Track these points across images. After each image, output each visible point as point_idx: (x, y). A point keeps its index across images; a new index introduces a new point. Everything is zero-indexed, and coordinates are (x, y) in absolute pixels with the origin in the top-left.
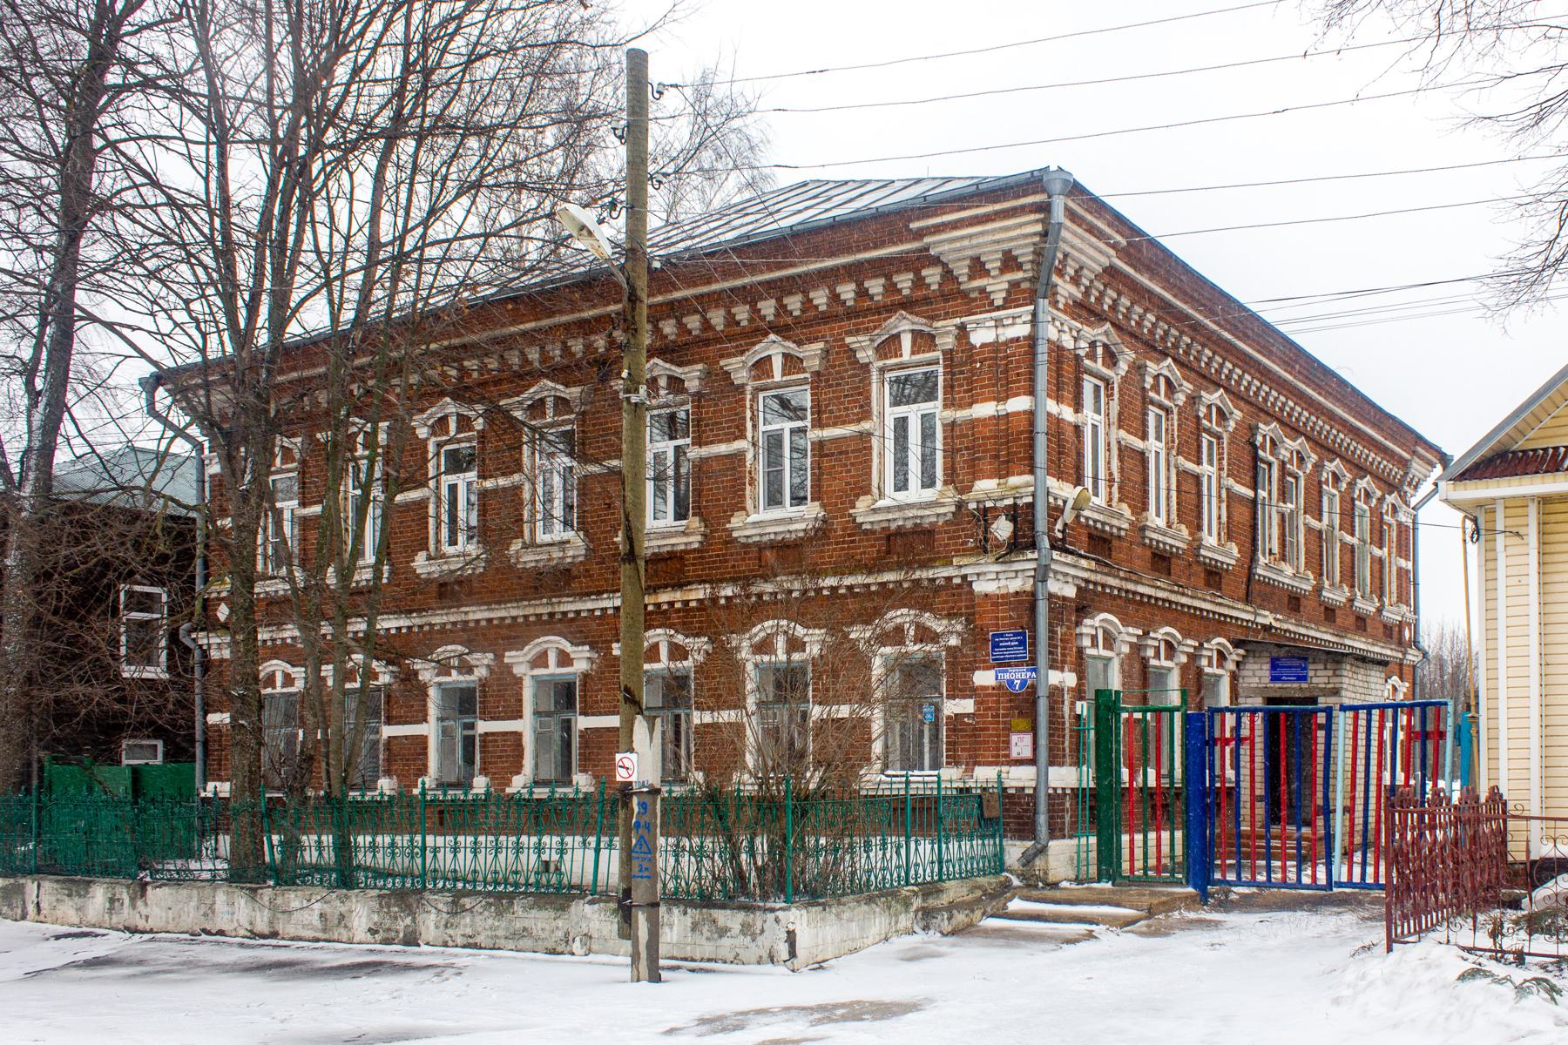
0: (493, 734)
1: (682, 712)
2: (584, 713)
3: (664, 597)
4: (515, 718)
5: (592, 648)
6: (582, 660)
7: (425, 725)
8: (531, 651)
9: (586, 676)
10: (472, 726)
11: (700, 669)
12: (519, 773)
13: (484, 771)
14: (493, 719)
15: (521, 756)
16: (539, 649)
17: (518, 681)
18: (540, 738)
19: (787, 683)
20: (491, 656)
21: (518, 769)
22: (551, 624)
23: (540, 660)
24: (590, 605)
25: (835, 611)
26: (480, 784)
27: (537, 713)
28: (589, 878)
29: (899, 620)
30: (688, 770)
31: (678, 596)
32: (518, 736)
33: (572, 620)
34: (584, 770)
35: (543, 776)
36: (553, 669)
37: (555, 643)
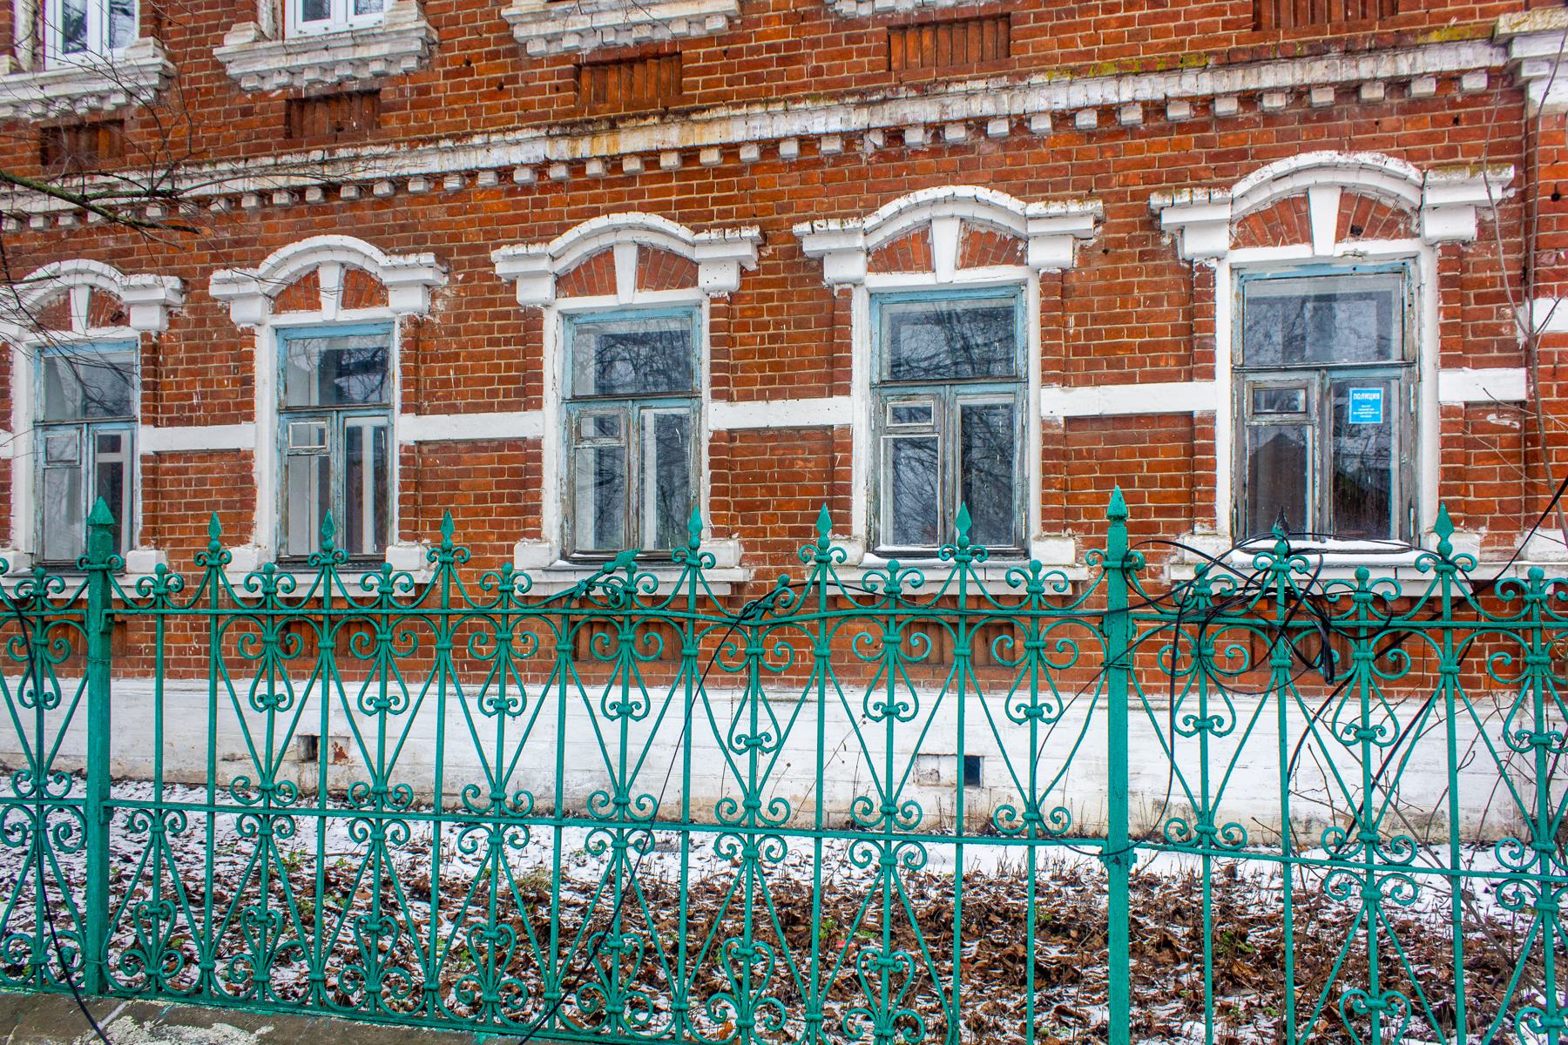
0: (175, 456)
1: (367, 423)
2: (413, 406)
3: (633, 141)
4: (235, 420)
5: (442, 257)
6: (412, 286)
7: (724, 425)
8: (575, 243)
9: (418, 329)
10: (113, 444)
11: (726, 310)
12: (241, 541)
13: (154, 534)
14: (172, 422)
15: (248, 503)
16: (592, 246)
17: (531, 321)
18: (289, 462)
19: (640, 365)
20: (174, 282)
21: (241, 530)
22: (326, 208)
23: (592, 274)
24: (434, 164)
25: (458, 227)
26: (143, 562)
27: (286, 410)
28: (672, 798)
29: (65, 281)
30: (381, 538)
31: (674, 136)
32: (241, 460)
33: (385, 202)
34: (411, 534)
35: (297, 549)
36: (947, 268)
37: (333, 252)
